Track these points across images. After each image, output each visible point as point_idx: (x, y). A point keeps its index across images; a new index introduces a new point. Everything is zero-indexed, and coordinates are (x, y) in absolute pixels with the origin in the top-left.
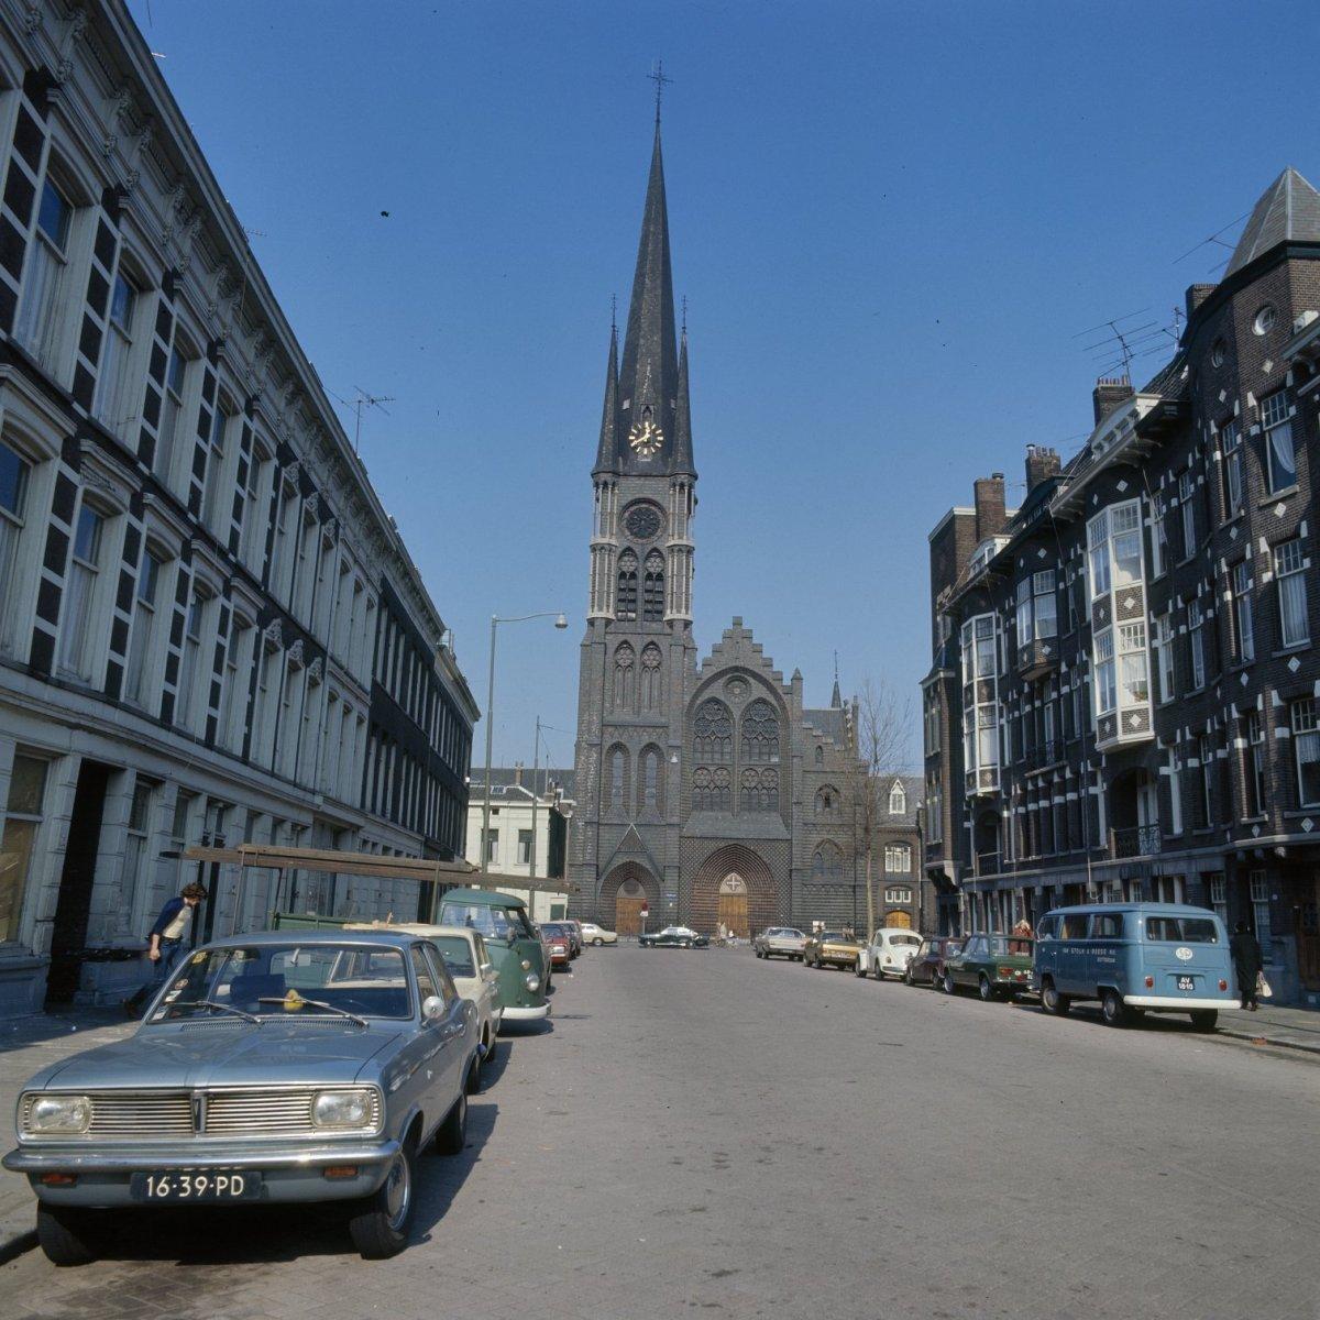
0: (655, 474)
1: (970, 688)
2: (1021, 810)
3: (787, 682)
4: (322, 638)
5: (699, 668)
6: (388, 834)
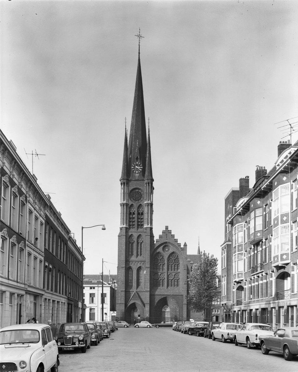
0: (140, 180)
1: (235, 247)
2: (250, 285)
3: (182, 246)
4: (24, 235)
5: (155, 243)
6: (54, 296)
